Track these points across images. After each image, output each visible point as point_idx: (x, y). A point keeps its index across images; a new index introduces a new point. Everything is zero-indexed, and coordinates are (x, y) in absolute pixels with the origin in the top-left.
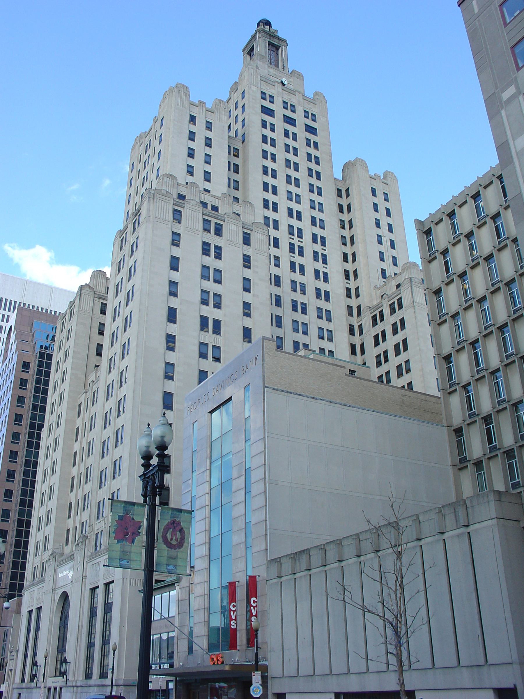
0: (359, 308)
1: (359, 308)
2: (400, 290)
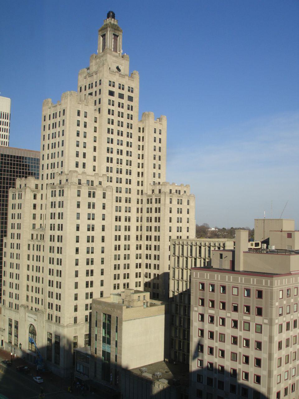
0: (142, 191)
1: (142, 191)
2: (160, 195)
